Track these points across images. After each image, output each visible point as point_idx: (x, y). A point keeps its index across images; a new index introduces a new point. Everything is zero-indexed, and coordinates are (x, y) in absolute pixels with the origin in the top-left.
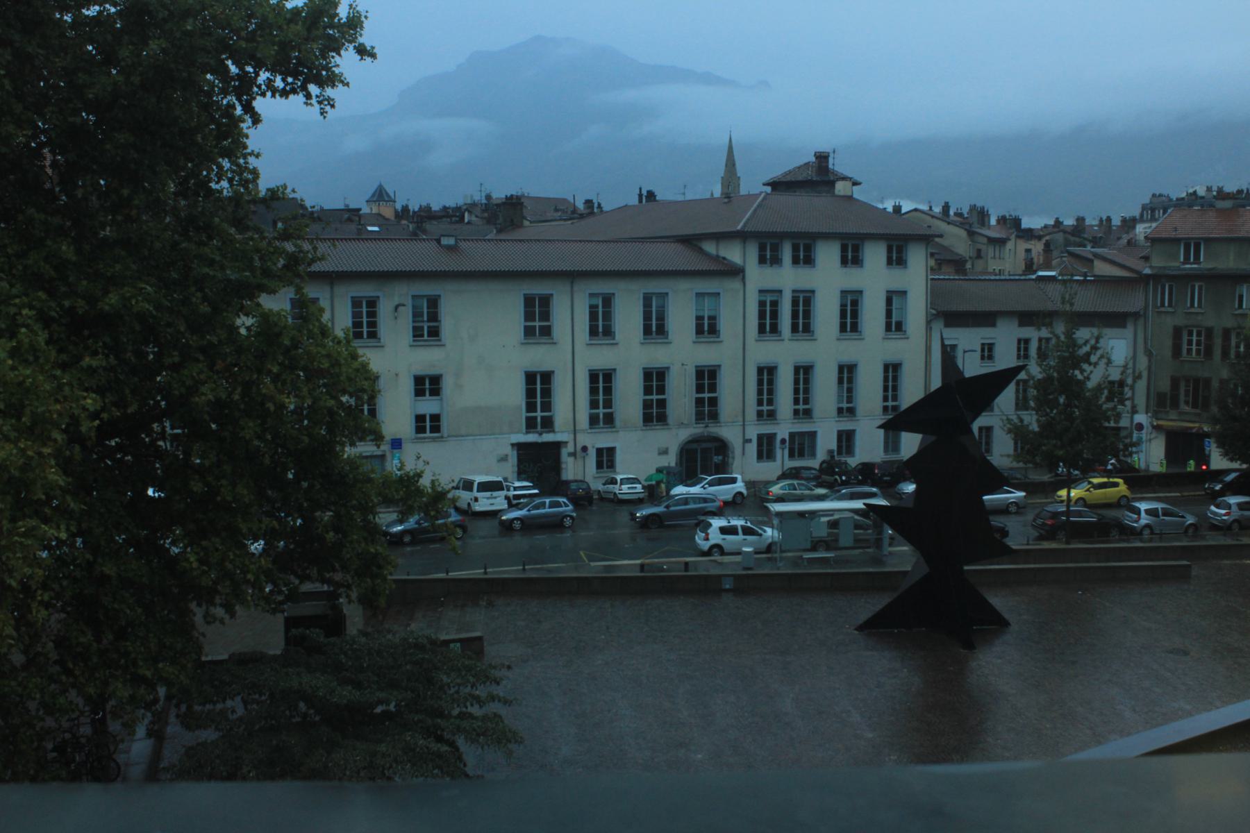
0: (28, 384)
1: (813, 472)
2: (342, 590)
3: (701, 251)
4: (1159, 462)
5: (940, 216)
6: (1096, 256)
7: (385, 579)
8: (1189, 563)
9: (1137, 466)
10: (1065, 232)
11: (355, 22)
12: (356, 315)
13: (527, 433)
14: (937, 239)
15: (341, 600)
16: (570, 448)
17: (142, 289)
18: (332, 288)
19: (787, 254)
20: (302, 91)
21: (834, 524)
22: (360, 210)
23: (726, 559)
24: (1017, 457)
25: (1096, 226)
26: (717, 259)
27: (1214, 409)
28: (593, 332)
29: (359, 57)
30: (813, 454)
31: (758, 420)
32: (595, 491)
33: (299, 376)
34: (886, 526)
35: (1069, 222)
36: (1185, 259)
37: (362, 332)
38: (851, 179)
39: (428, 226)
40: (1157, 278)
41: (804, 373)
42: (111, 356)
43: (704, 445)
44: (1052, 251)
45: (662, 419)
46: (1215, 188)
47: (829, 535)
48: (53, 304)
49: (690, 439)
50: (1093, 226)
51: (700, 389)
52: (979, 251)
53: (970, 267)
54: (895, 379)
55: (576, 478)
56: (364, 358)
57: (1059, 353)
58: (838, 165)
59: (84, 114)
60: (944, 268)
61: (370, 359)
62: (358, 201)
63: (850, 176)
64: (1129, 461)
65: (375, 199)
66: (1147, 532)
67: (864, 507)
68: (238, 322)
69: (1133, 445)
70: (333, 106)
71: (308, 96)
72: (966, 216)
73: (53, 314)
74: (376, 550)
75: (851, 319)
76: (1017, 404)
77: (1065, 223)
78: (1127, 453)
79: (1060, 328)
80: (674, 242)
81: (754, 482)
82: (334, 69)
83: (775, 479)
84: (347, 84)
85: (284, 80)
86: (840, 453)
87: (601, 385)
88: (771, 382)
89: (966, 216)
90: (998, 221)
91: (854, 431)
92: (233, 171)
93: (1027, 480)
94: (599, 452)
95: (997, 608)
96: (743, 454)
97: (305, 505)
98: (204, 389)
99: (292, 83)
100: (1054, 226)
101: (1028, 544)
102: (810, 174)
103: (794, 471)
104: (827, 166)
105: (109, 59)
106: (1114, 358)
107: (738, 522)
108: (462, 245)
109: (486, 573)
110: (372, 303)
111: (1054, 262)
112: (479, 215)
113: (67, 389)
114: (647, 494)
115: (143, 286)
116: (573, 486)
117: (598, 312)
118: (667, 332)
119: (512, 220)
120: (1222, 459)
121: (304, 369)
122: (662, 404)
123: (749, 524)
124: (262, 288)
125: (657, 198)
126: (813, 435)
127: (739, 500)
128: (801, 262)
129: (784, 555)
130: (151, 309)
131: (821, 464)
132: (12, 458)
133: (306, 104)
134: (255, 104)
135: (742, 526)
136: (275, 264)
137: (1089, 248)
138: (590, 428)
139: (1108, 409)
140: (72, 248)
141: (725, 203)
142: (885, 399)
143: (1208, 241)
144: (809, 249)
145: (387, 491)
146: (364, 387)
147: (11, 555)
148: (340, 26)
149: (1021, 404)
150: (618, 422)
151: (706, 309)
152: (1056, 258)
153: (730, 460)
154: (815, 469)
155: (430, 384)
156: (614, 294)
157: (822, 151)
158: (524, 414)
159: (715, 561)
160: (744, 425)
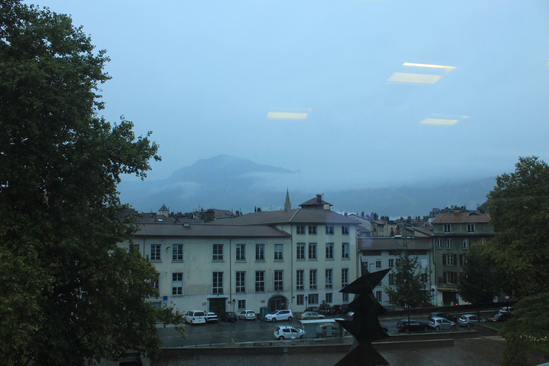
0: (29, 272)
1: (317, 309)
2: (142, 352)
3: (276, 229)
4: (441, 303)
5: (361, 217)
6: (414, 229)
7: (158, 348)
8: (453, 340)
9: (433, 305)
10: (404, 222)
11: (155, 148)
12: (153, 251)
13: (213, 294)
14: (360, 225)
15: (141, 356)
16: (229, 300)
17: (74, 239)
18: (144, 241)
19: (307, 230)
20: (135, 171)
21: (325, 328)
22: (156, 213)
23: (286, 341)
24: (390, 302)
25: (415, 219)
26: (282, 232)
27: (459, 283)
28: (238, 258)
29: (156, 160)
30: (317, 302)
31: (297, 290)
32: (238, 316)
33: (129, 272)
34: (343, 328)
35: (405, 218)
36: (445, 230)
37: (155, 257)
38: (329, 204)
39: (180, 219)
40: (436, 237)
41: (313, 273)
42: (61, 263)
43: (278, 299)
44: (399, 228)
45: (262, 289)
46: (454, 206)
47: (323, 332)
48: (41, 244)
49: (272, 297)
50: (414, 219)
51: (276, 278)
52: (375, 229)
53: (372, 234)
54: (346, 274)
55: (231, 311)
56: (153, 266)
57: (403, 264)
58: (324, 199)
59: (59, 178)
60: (363, 235)
61: (155, 266)
62: (156, 210)
63: (329, 203)
64: (430, 303)
65: (162, 210)
66: (437, 328)
67: (335, 321)
68: (109, 252)
69: (431, 297)
70: (146, 177)
71: (138, 173)
72: (370, 216)
73: (41, 247)
74: (155, 337)
75: (330, 253)
76: (390, 283)
77: (404, 219)
78: (429, 300)
79: (403, 255)
80: (267, 226)
81: (296, 312)
82: (147, 164)
83: (304, 311)
84: (151, 169)
85: (129, 167)
86: (327, 301)
87: (240, 277)
88: (302, 276)
89: (370, 216)
90: (381, 218)
91: (332, 293)
92: (110, 199)
93: (394, 310)
94: (240, 301)
95: (384, 358)
96: (292, 302)
97: (129, 320)
98: (94, 276)
99: (132, 169)
100: (400, 220)
101: (395, 334)
102: (315, 202)
103: (310, 308)
104: (321, 200)
105: (70, 160)
106: (422, 265)
107: (290, 327)
108: (192, 226)
109: (196, 347)
110: (159, 247)
111: (401, 233)
112: (198, 216)
113: (43, 274)
114: (257, 317)
115: (75, 238)
116: (230, 314)
117: (239, 251)
118: (264, 258)
119: (210, 218)
120: (462, 301)
121: (131, 269)
122: (262, 284)
123: (294, 328)
124: (118, 240)
125: (261, 210)
126: (317, 295)
127: (290, 319)
128: (312, 233)
129: (307, 339)
130: (77, 246)
131: (320, 306)
132: (20, 300)
133: (137, 176)
134: (119, 175)
135: (291, 329)
136: (123, 232)
137: (413, 227)
138: (236, 293)
139: (421, 284)
140: (51, 224)
141: (285, 212)
142: (343, 282)
143: (452, 224)
144: (315, 228)
145: (160, 315)
146: (153, 276)
147: (16, 337)
148: (149, 150)
149: (391, 283)
150: (246, 291)
151: (278, 249)
152: (402, 231)
153: (287, 305)
154: (318, 308)
155: (178, 276)
156: (245, 244)
157: (319, 194)
158: (212, 288)
159: (281, 342)
160: (292, 292)
